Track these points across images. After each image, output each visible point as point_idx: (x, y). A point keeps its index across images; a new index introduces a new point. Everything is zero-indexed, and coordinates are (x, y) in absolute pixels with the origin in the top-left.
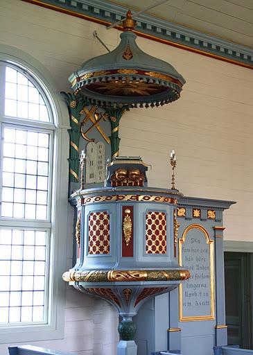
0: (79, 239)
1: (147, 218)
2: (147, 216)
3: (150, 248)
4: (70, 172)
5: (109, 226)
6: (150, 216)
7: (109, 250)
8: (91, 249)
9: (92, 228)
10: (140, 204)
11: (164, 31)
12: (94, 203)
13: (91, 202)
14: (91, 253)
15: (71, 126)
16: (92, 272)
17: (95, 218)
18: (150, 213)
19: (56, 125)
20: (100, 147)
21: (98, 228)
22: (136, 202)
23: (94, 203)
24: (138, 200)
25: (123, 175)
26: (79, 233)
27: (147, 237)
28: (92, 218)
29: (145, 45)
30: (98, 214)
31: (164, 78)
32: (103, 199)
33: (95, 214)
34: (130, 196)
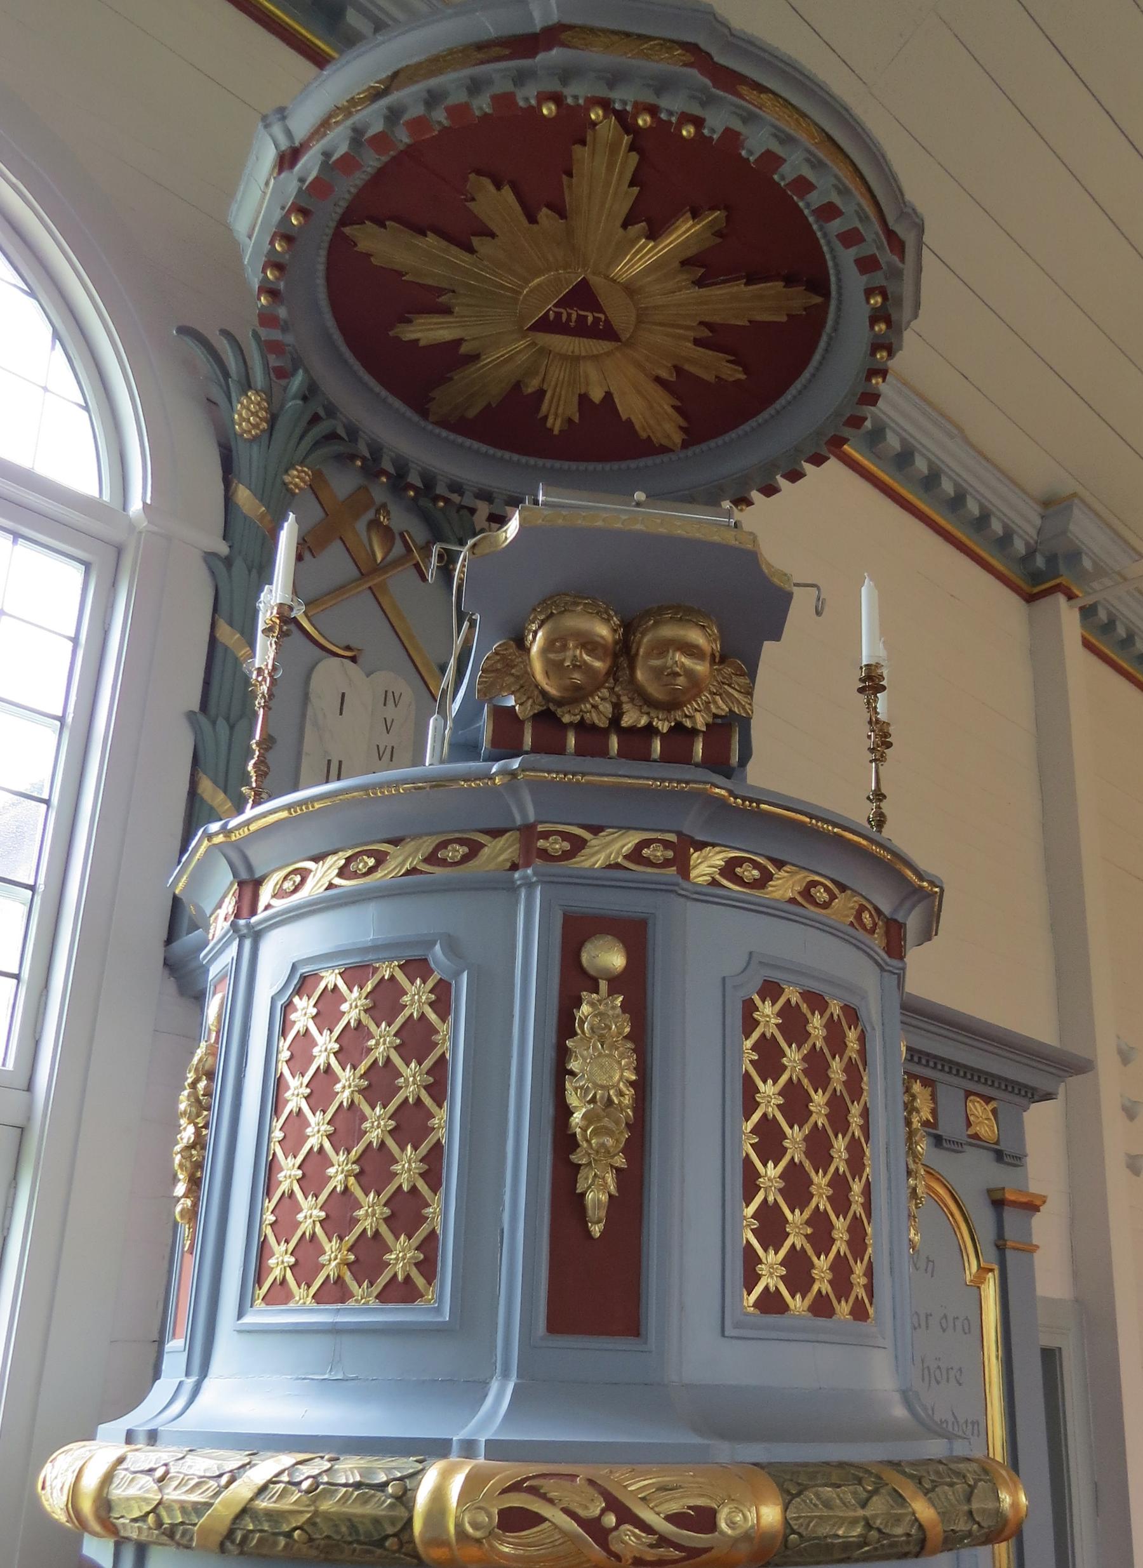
0: (195, 1183)
1: (751, 1280)
2: (749, 1008)
3: (771, 1275)
4: (213, 641)
5: (440, 1070)
6: (768, 1012)
7: (428, 1265)
8: (280, 1258)
9: (289, 1170)
10: (695, 910)
11: (904, 458)
12: (331, 902)
13: (313, 889)
14: (279, 1294)
15: (225, 537)
16: (265, 1469)
17: (326, 1016)
18: (771, 990)
19: (136, 506)
20: (389, 697)
21: (346, 1084)
22: (668, 889)
23: (331, 902)
24: (684, 870)
25: (590, 644)
26: (199, 1142)
27: (751, 1184)
28: (304, 1011)
29: (763, 806)
30: (354, 974)
31: (854, 205)
32: (399, 861)
33: (331, 978)
34: (630, 841)
